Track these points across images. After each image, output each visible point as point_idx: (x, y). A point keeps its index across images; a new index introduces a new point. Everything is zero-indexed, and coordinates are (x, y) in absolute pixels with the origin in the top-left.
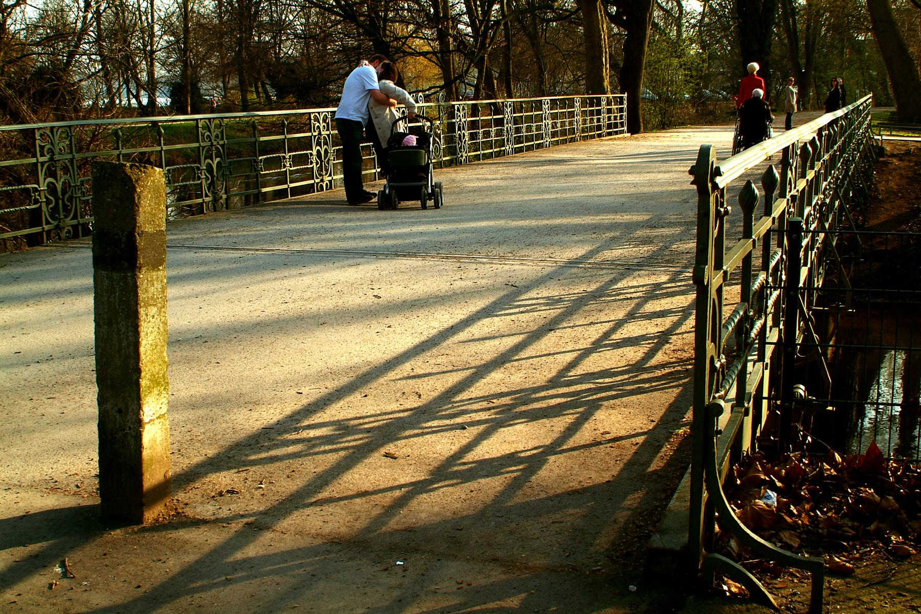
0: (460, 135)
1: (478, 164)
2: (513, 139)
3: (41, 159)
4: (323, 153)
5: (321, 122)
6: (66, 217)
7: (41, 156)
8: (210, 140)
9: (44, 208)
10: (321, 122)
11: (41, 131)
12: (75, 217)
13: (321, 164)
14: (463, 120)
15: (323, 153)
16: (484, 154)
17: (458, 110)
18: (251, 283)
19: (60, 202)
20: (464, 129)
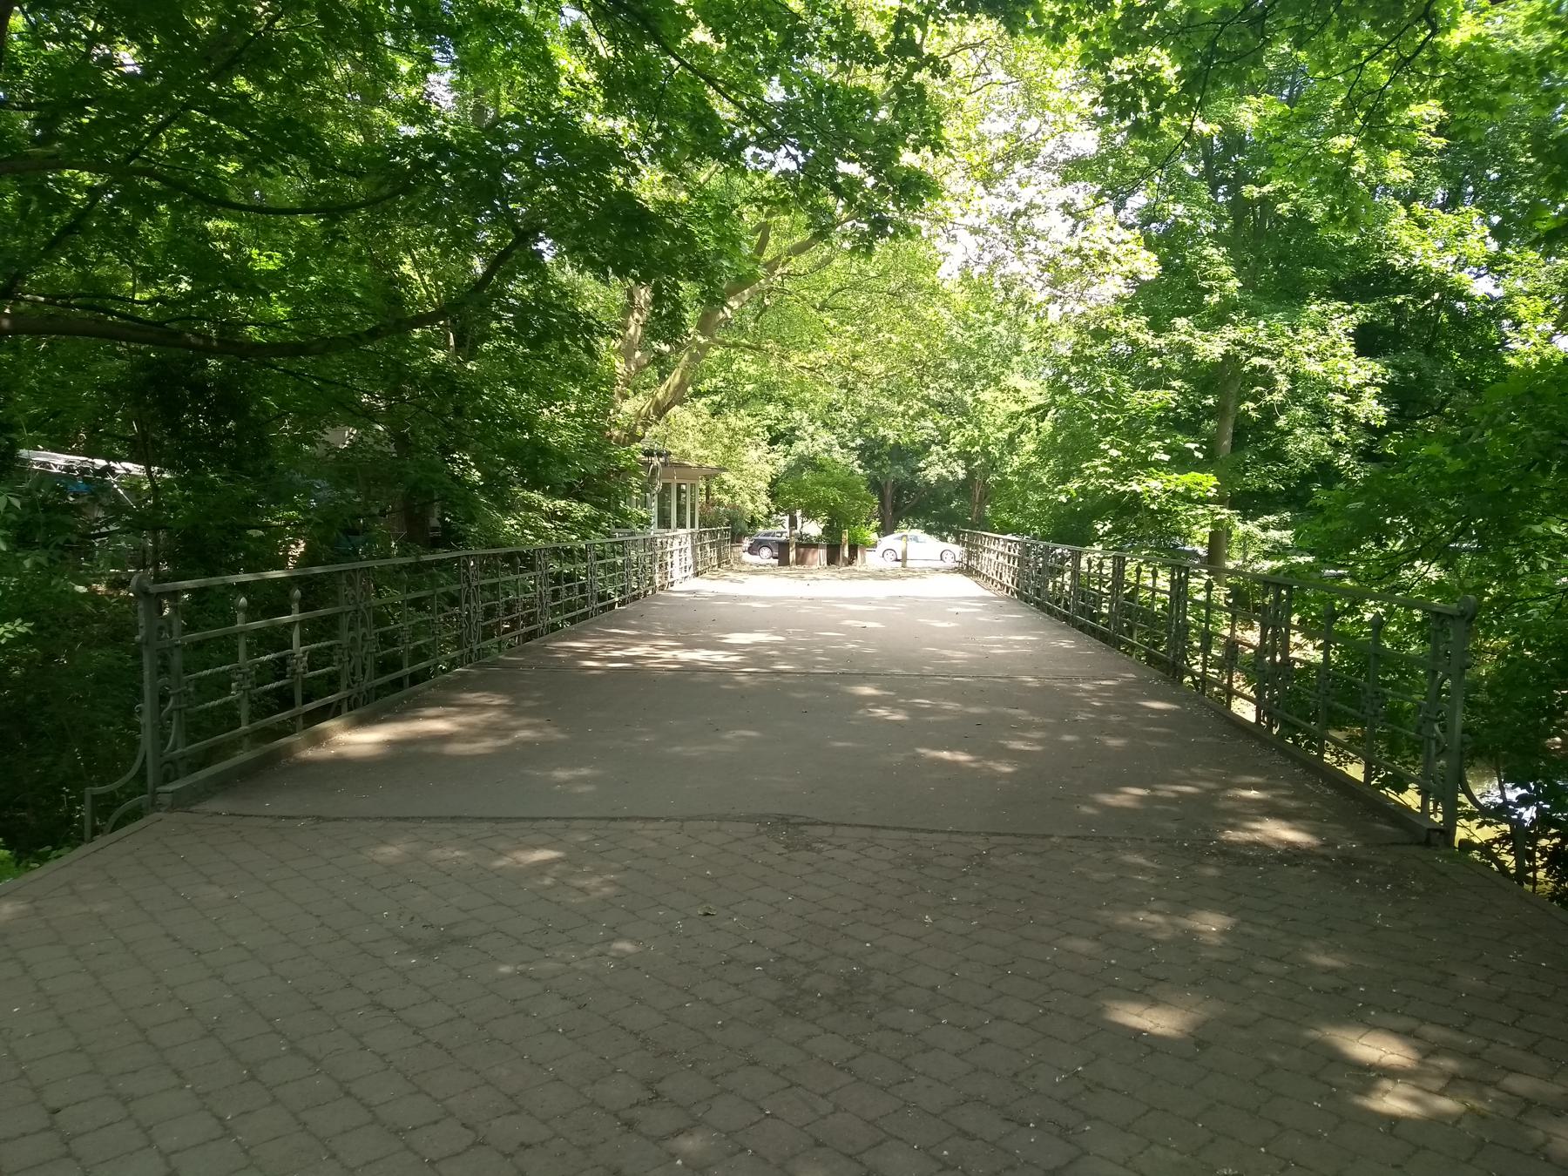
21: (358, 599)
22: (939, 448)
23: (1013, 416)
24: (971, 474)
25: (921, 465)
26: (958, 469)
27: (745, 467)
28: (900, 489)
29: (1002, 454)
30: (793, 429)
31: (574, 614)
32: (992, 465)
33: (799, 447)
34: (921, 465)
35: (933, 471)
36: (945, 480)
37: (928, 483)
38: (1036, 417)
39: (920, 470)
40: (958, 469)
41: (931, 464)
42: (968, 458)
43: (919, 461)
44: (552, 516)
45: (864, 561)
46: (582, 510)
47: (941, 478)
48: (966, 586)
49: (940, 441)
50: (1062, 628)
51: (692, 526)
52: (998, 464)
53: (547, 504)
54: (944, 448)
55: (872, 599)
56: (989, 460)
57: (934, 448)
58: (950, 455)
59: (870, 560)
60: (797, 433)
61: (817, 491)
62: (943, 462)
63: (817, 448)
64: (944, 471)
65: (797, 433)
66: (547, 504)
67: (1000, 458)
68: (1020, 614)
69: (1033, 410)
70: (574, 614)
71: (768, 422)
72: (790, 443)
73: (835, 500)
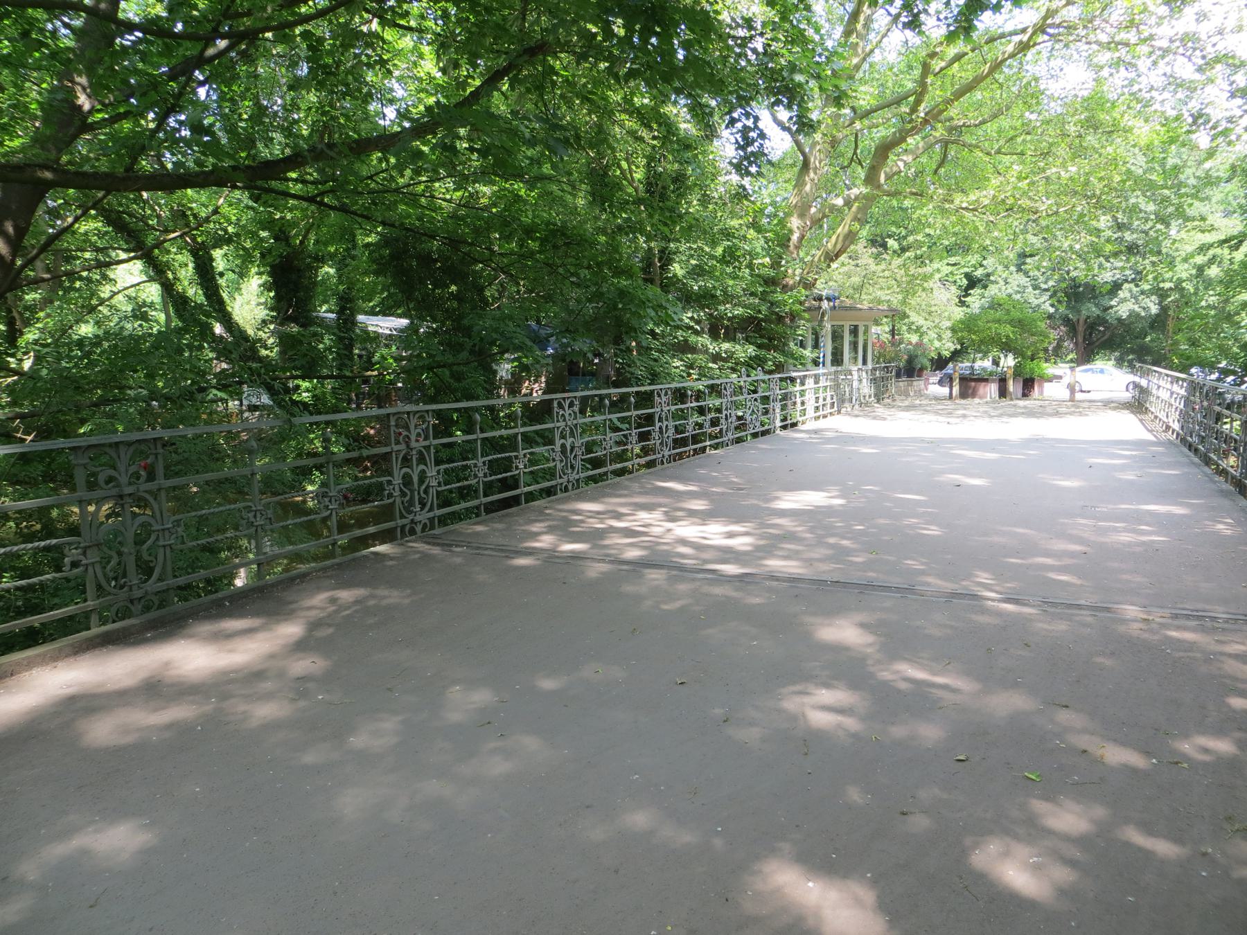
0: (563, 446)
1: (557, 500)
2: (670, 442)
3: (396, 448)
4: (415, 479)
5: (566, 408)
6: (422, 509)
7: (396, 444)
8: (564, 420)
9: (398, 500)
10: (566, 408)
11: (396, 417)
12: (578, 473)
13: (566, 463)
14: (665, 409)
15: (415, 479)
16: (695, 450)
17: (725, 389)
18: (300, 659)
19: (416, 493)
20: (667, 420)
21: (567, 418)
22: (1132, 285)
23: (1203, 249)
24: (1164, 310)
25: (1113, 303)
26: (1151, 305)
27: (933, 309)
28: (1092, 325)
29: (1197, 289)
30: (988, 275)
31: (458, 485)
32: (1186, 300)
33: (993, 290)
34: (1113, 303)
35: (1123, 306)
36: (1138, 315)
37: (1119, 320)
38: (1230, 247)
39: (1112, 307)
40: (1151, 305)
41: (1124, 300)
42: (1162, 294)
43: (1112, 299)
44: (716, 358)
45: (1041, 393)
46: (745, 351)
47: (1132, 314)
48: (1129, 427)
49: (1133, 280)
50: (1223, 493)
51: (865, 362)
52: (1193, 299)
53: (713, 347)
54: (1137, 286)
55: (1115, 408)
56: (1182, 296)
57: (1126, 286)
58: (1143, 292)
59: (1052, 391)
60: (992, 278)
61: (989, 328)
62: (1136, 298)
63: (1010, 291)
64: (1136, 308)
65: (992, 278)
66: (713, 347)
67: (1196, 294)
68: (1180, 469)
69: (1225, 241)
70: (458, 485)
71: (966, 270)
72: (985, 287)
73: (1007, 337)
